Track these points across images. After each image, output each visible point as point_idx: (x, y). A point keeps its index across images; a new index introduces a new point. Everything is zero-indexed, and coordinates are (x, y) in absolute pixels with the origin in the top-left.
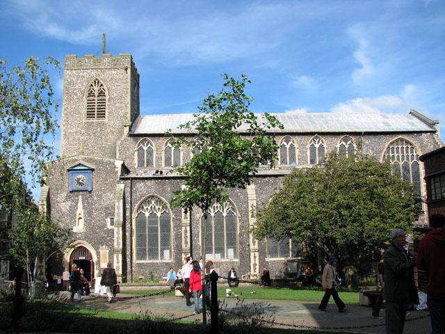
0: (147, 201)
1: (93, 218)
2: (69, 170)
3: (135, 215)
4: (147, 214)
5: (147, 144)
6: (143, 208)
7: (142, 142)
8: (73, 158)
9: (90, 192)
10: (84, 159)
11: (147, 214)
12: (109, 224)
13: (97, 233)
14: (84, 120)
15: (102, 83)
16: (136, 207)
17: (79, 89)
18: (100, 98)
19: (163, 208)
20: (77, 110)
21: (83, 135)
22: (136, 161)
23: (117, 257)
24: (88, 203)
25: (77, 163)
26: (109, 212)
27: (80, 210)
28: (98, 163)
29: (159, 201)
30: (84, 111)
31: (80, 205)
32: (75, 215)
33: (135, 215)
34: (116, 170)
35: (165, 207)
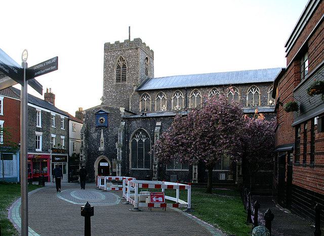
0: (137, 133)
3: (131, 141)
4: (137, 140)
9: (107, 127)
10: (103, 107)
11: (137, 140)
16: (131, 136)
19: (146, 137)
20: (111, 77)
22: (140, 108)
23: (118, 165)
26: (116, 139)
27: (102, 138)
28: (111, 109)
29: (144, 132)
31: (102, 135)
33: (131, 141)
35: (147, 136)
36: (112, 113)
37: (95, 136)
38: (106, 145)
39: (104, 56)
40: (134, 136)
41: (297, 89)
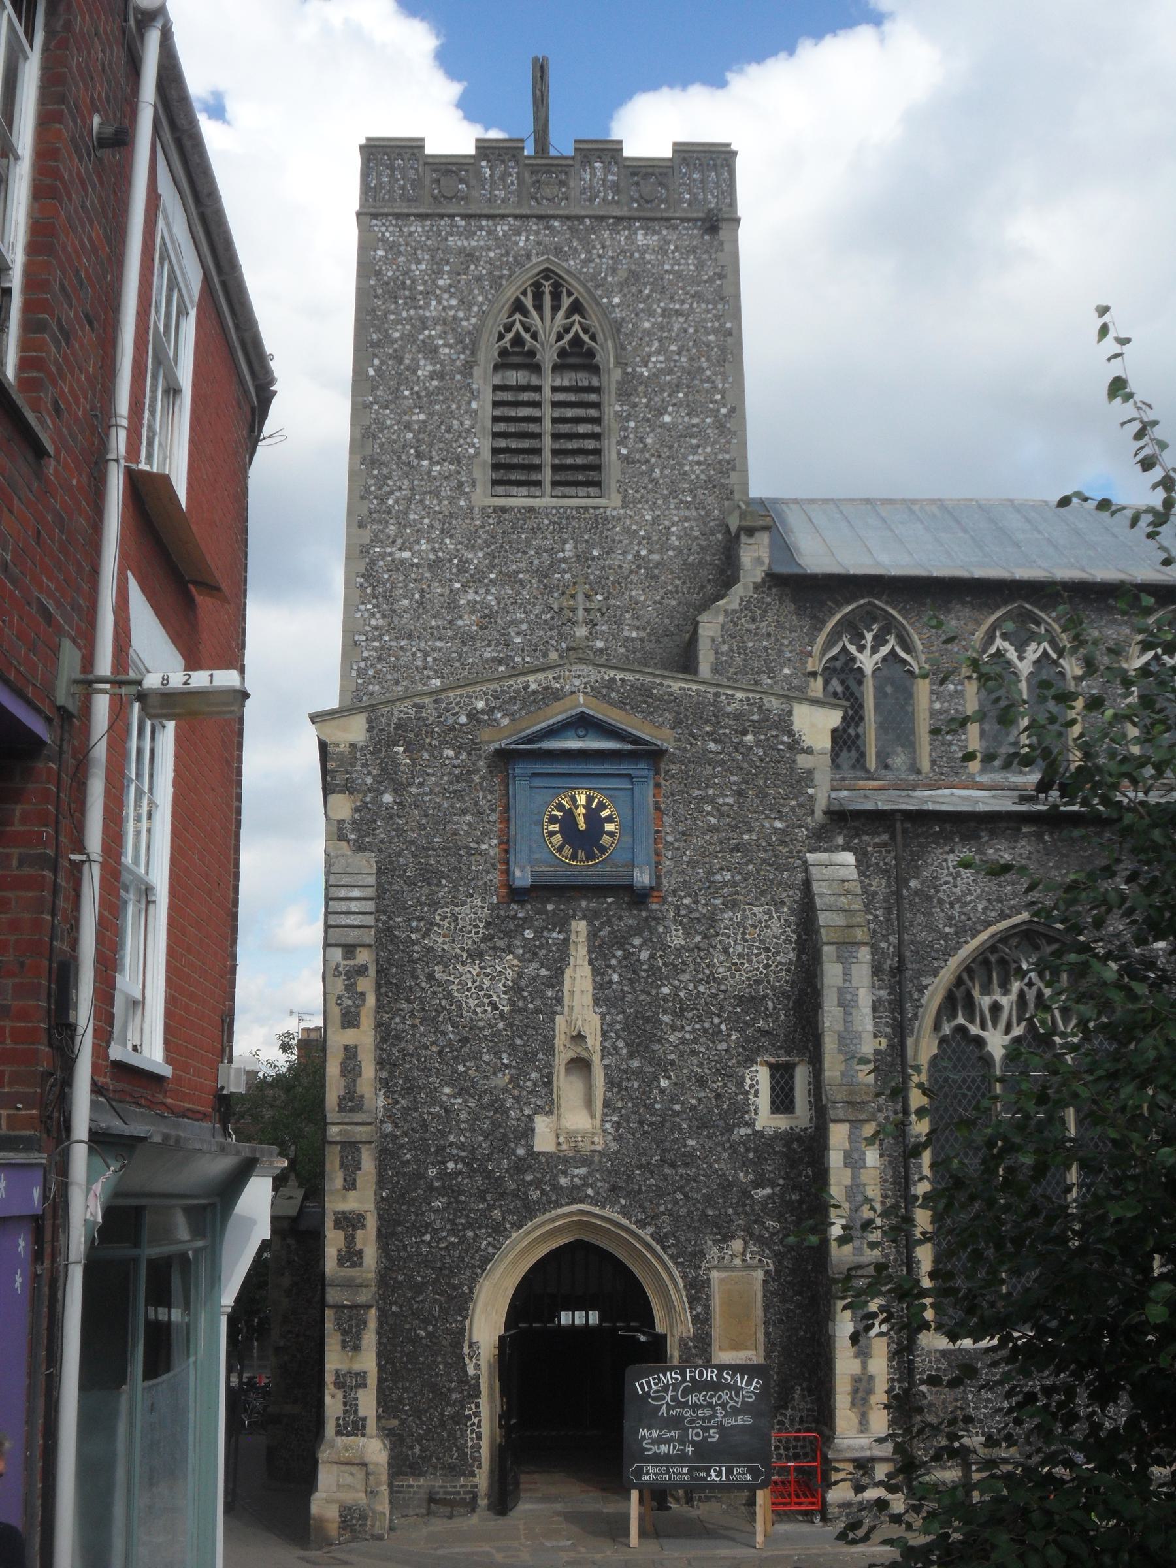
1: (664, 1067)
2: (505, 758)
4: (996, 1043)
5: (879, 641)
6: (970, 1006)
7: (852, 628)
8: (534, 682)
11: (996, 1043)
12: (763, 1100)
13: (689, 1159)
14: (482, 497)
15: (579, 291)
17: (449, 324)
18: (565, 380)
21: (476, 580)
24: (630, 964)
25: (556, 714)
27: (580, 1007)
30: (482, 445)
31: (579, 979)
32: (549, 1048)
34: (803, 761)
36: (705, 758)
37: (480, 986)
38: (627, 1097)
39: (364, 248)
40: (957, 1000)
41: (151, 776)
